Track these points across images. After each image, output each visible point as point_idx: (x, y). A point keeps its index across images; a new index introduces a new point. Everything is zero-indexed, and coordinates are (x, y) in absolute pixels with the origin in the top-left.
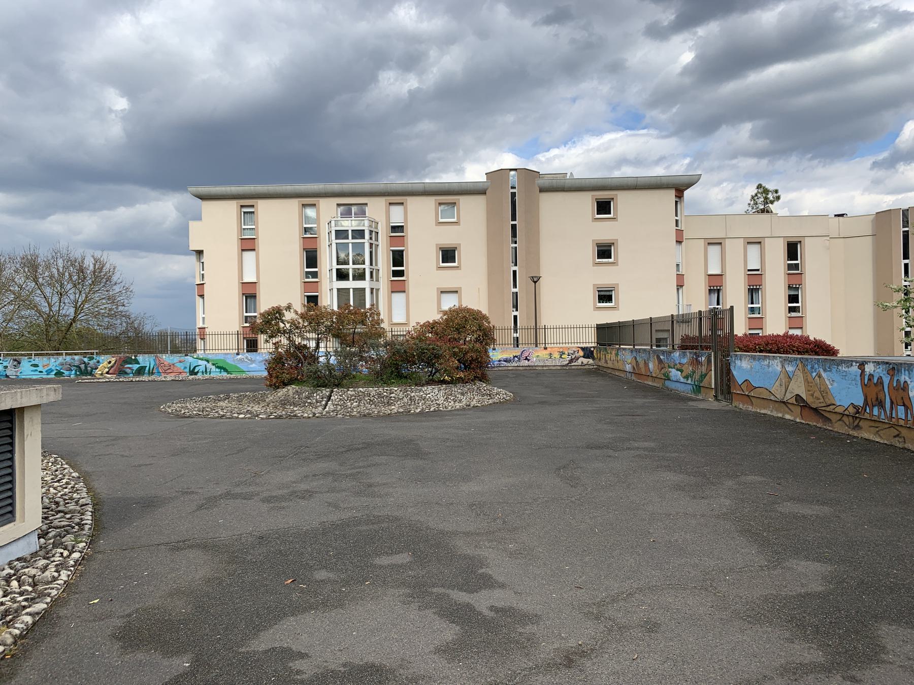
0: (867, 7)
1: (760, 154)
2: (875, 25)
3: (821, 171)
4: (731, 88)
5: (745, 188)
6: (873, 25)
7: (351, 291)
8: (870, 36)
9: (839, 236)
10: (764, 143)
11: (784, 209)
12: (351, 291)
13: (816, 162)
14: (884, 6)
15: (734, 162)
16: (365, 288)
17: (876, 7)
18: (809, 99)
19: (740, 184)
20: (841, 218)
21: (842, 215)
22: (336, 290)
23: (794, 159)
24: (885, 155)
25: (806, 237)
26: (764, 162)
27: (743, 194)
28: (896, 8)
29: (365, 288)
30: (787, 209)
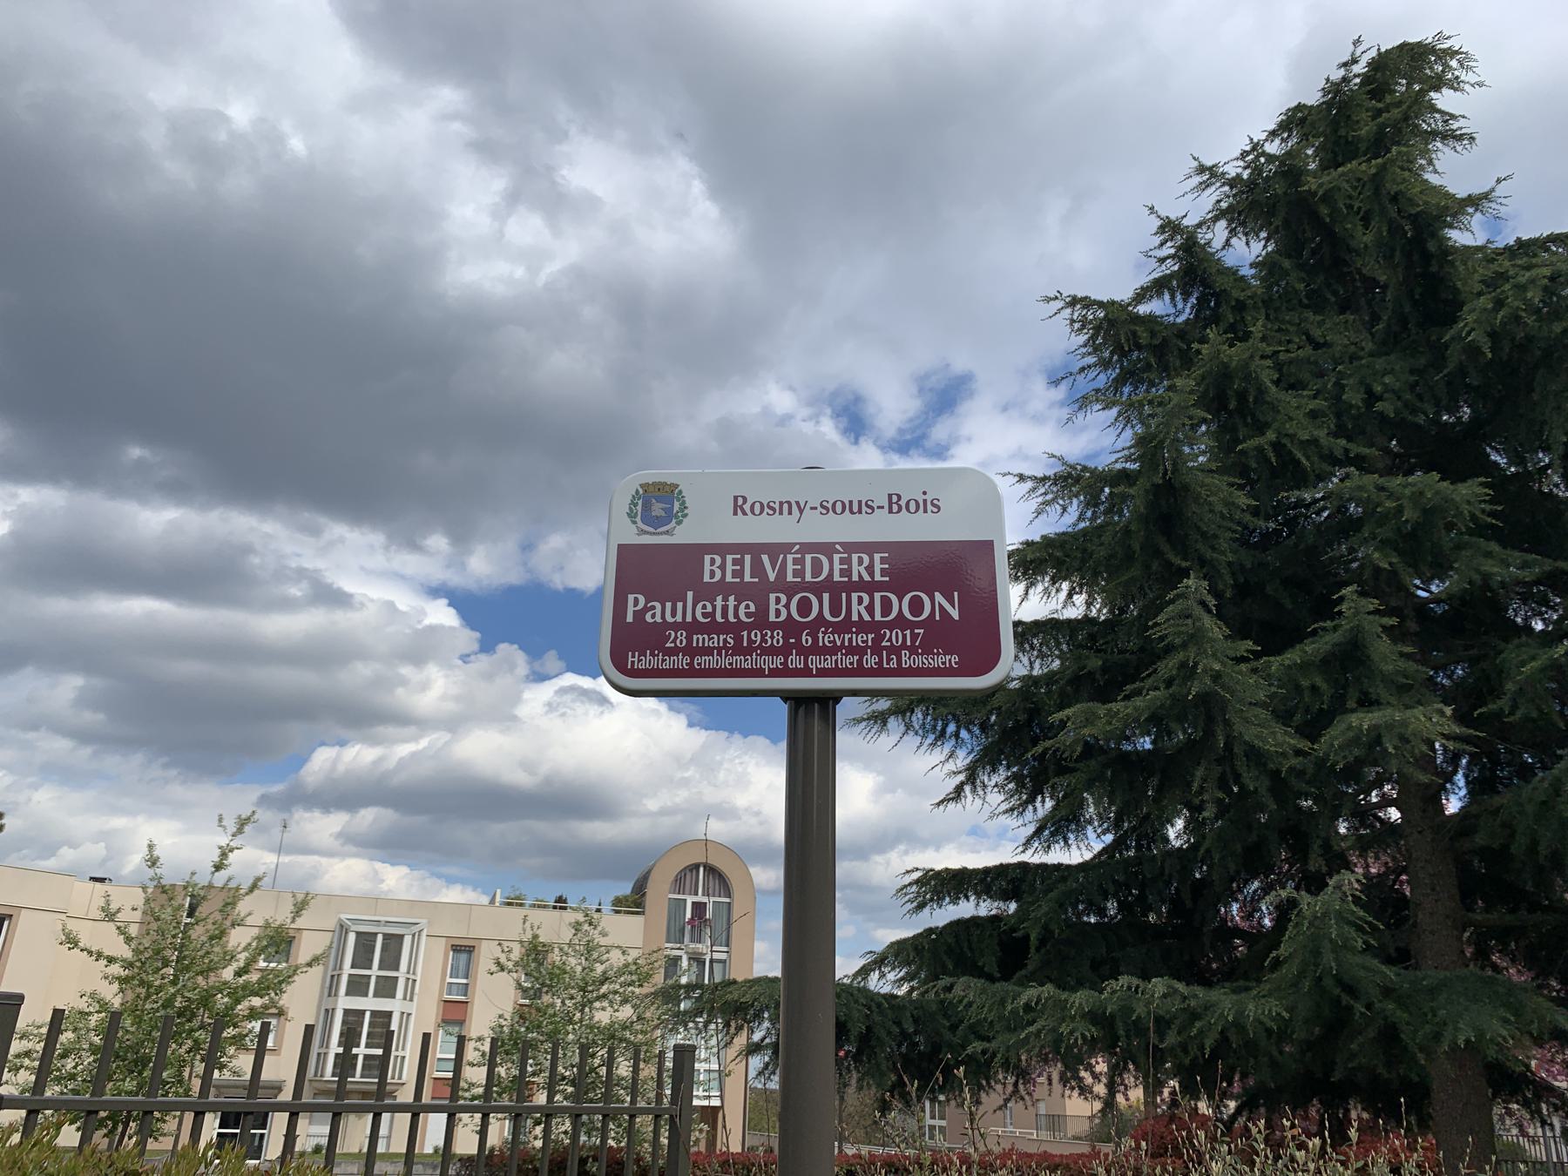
0: (294, 565)
1: (83, 736)
2: (299, 594)
3: (178, 791)
4: (59, 607)
5: (36, 790)
6: (295, 591)
7: (368, 1015)
8: (287, 605)
9: (87, 915)
10: (92, 718)
11: (97, 843)
12: (368, 1015)
13: (173, 772)
14: (316, 571)
15: (31, 735)
16: (391, 1012)
17: (306, 569)
18: (188, 669)
19: (31, 780)
20: (98, 885)
21: (102, 880)
22: (342, 1012)
23: (138, 758)
24: (277, 788)
25: (23, 910)
26: (86, 751)
27: (30, 800)
28: (330, 581)
29: (391, 1012)
30: (103, 844)
